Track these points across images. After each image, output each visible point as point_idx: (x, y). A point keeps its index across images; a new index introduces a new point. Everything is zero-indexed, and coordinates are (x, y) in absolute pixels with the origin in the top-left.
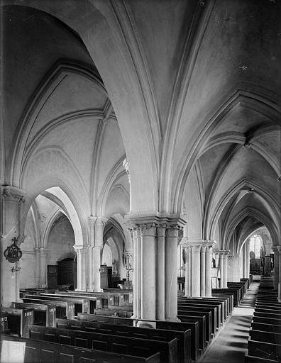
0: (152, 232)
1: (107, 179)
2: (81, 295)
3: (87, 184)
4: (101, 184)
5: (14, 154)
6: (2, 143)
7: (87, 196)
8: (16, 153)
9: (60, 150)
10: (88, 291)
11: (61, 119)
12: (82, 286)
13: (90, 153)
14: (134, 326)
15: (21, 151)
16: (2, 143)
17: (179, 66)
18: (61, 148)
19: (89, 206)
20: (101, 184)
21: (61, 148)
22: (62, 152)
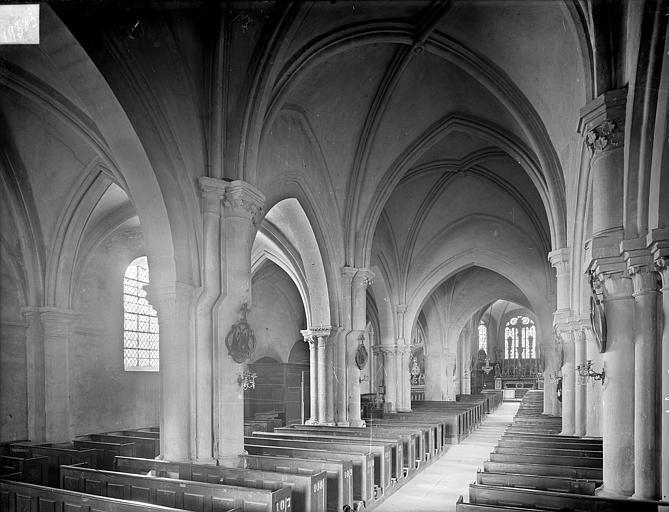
0: (618, 85)
1: (379, 190)
2: (325, 433)
3: (341, 197)
4: (366, 199)
5: (250, 105)
6: (393, 3)
7: (340, 227)
8: (254, 105)
9: (301, 117)
10: (340, 424)
11: (334, 36)
12: (327, 415)
13: (356, 127)
14: (507, 358)
15: (264, 101)
16: (393, 3)
17: (251, 88)
18: (304, 113)
19: (342, 245)
20: (366, 199)
21: (304, 113)
22: (304, 122)
